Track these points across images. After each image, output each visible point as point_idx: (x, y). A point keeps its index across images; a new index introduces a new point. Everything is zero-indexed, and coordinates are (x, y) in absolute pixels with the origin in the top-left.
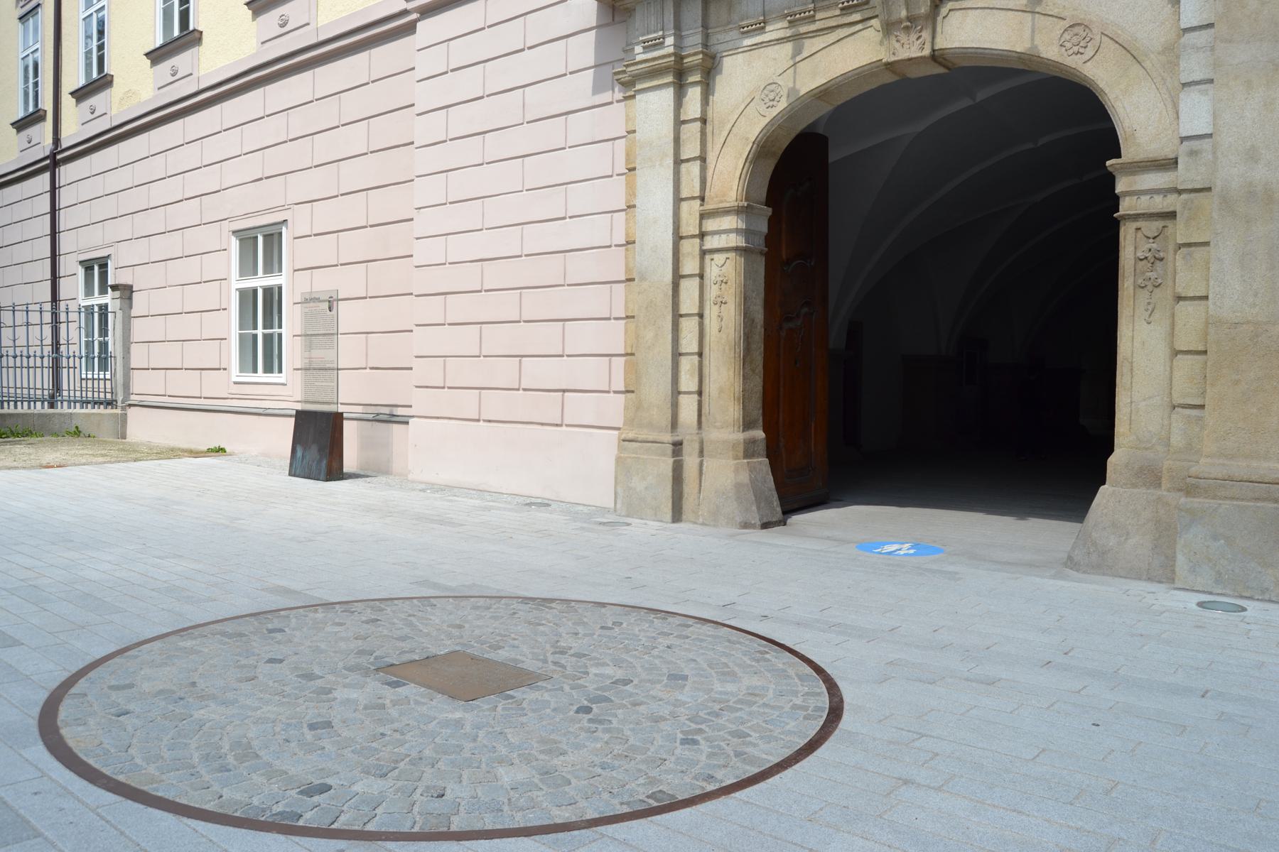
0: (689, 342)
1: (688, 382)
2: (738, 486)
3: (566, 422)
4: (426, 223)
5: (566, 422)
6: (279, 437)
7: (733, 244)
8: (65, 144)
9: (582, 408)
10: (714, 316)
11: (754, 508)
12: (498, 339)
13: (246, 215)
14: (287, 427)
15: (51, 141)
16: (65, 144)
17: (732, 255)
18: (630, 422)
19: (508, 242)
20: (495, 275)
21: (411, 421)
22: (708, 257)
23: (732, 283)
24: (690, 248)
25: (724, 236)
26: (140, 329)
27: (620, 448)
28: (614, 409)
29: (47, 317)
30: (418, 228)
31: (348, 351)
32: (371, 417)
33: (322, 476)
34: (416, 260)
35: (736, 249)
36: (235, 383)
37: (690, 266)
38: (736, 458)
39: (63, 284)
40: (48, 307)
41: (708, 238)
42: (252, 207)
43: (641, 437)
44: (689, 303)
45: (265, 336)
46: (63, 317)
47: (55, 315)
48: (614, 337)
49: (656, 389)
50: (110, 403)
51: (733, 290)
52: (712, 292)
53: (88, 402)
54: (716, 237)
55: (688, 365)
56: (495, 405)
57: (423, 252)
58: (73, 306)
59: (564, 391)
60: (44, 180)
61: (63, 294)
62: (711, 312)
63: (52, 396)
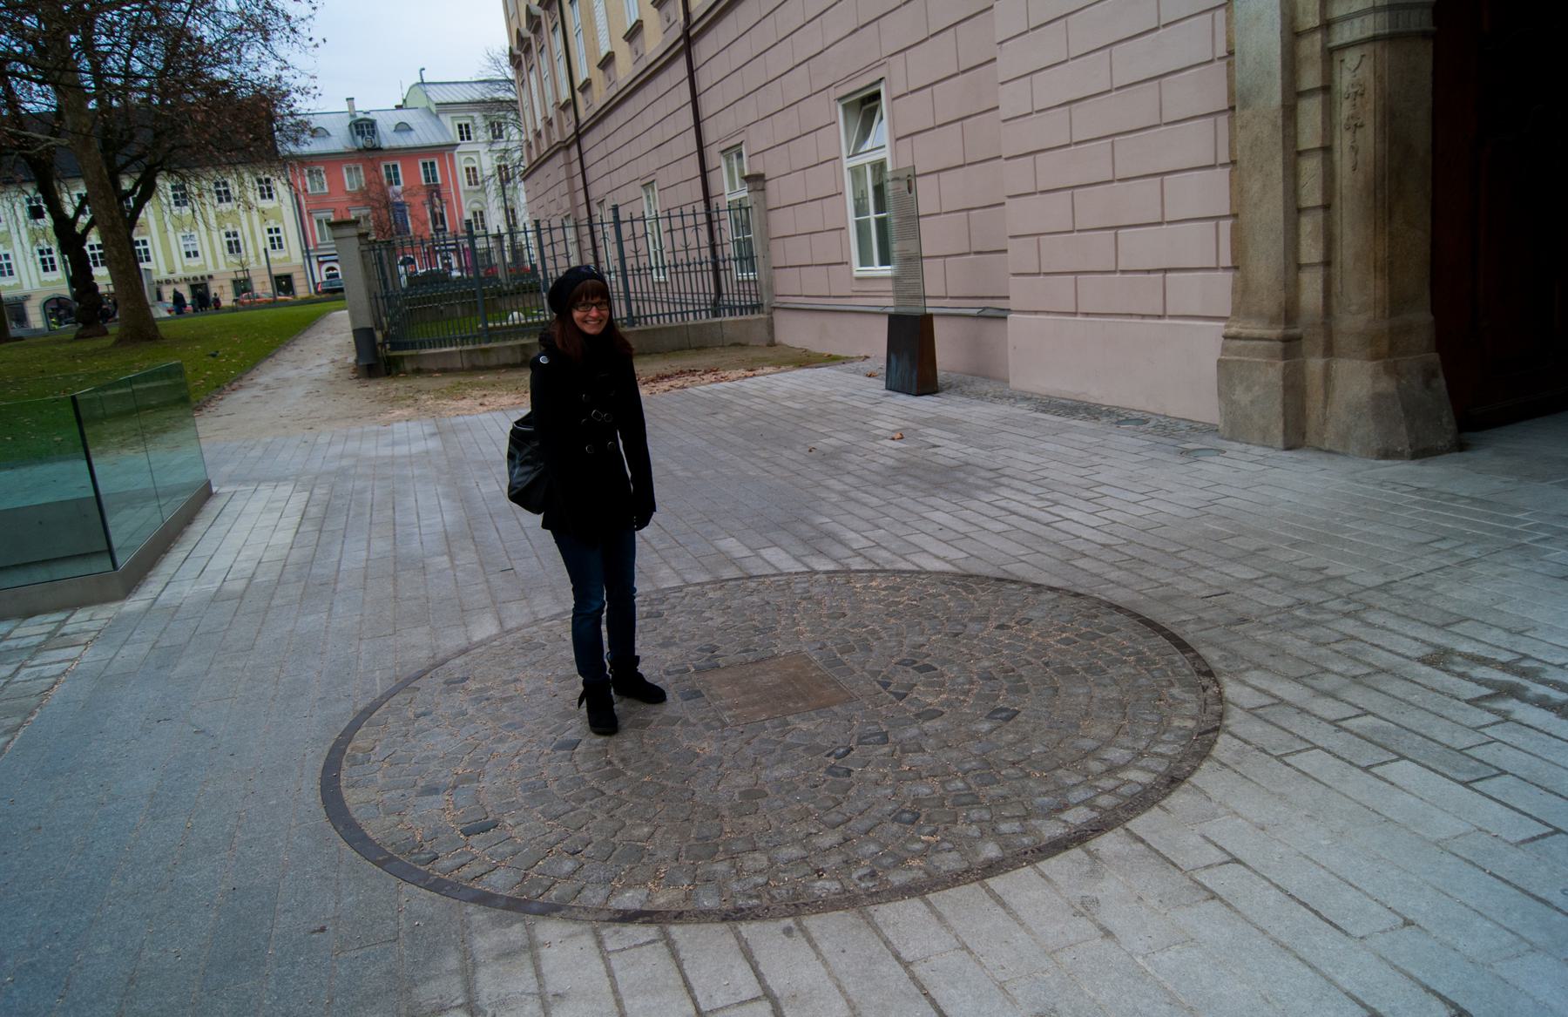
0: (1311, 195)
1: (1311, 251)
2: (1378, 398)
3: (1169, 312)
4: (1011, 61)
5: (1169, 312)
6: (875, 340)
7: (1369, 33)
8: (695, 17)
9: (1190, 292)
10: (1346, 149)
11: (1403, 429)
12: (1093, 207)
13: (850, 78)
14: (881, 328)
15: (682, 18)
16: (695, 17)
17: (1368, 49)
18: (1236, 310)
19: (1092, 74)
20: (1089, 120)
21: (1010, 316)
22: (1337, 57)
23: (1370, 94)
24: (1311, 47)
25: (1357, 22)
26: (781, 222)
27: (1225, 349)
28: (1219, 290)
29: (702, 219)
30: (1003, 69)
31: (934, 236)
32: (975, 312)
33: (914, 390)
34: (1004, 113)
35: (1374, 39)
36: (858, 279)
37: (1310, 77)
38: (1375, 357)
39: (712, 177)
40: (700, 207)
41: (1337, 28)
42: (847, 67)
43: (1246, 332)
44: (1310, 133)
45: (878, 220)
46: (715, 216)
47: (709, 216)
48: (1213, 192)
49: (1266, 265)
50: (756, 308)
51: (1370, 106)
52: (1344, 111)
53: (746, 307)
54: (1347, 26)
55: (1309, 226)
56: (1094, 292)
57: (1012, 100)
58: (723, 206)
59: (1166, 271)
60: (680, 69)
61: (713, 191)
62: (1343, 141)
63: (715, 303)
